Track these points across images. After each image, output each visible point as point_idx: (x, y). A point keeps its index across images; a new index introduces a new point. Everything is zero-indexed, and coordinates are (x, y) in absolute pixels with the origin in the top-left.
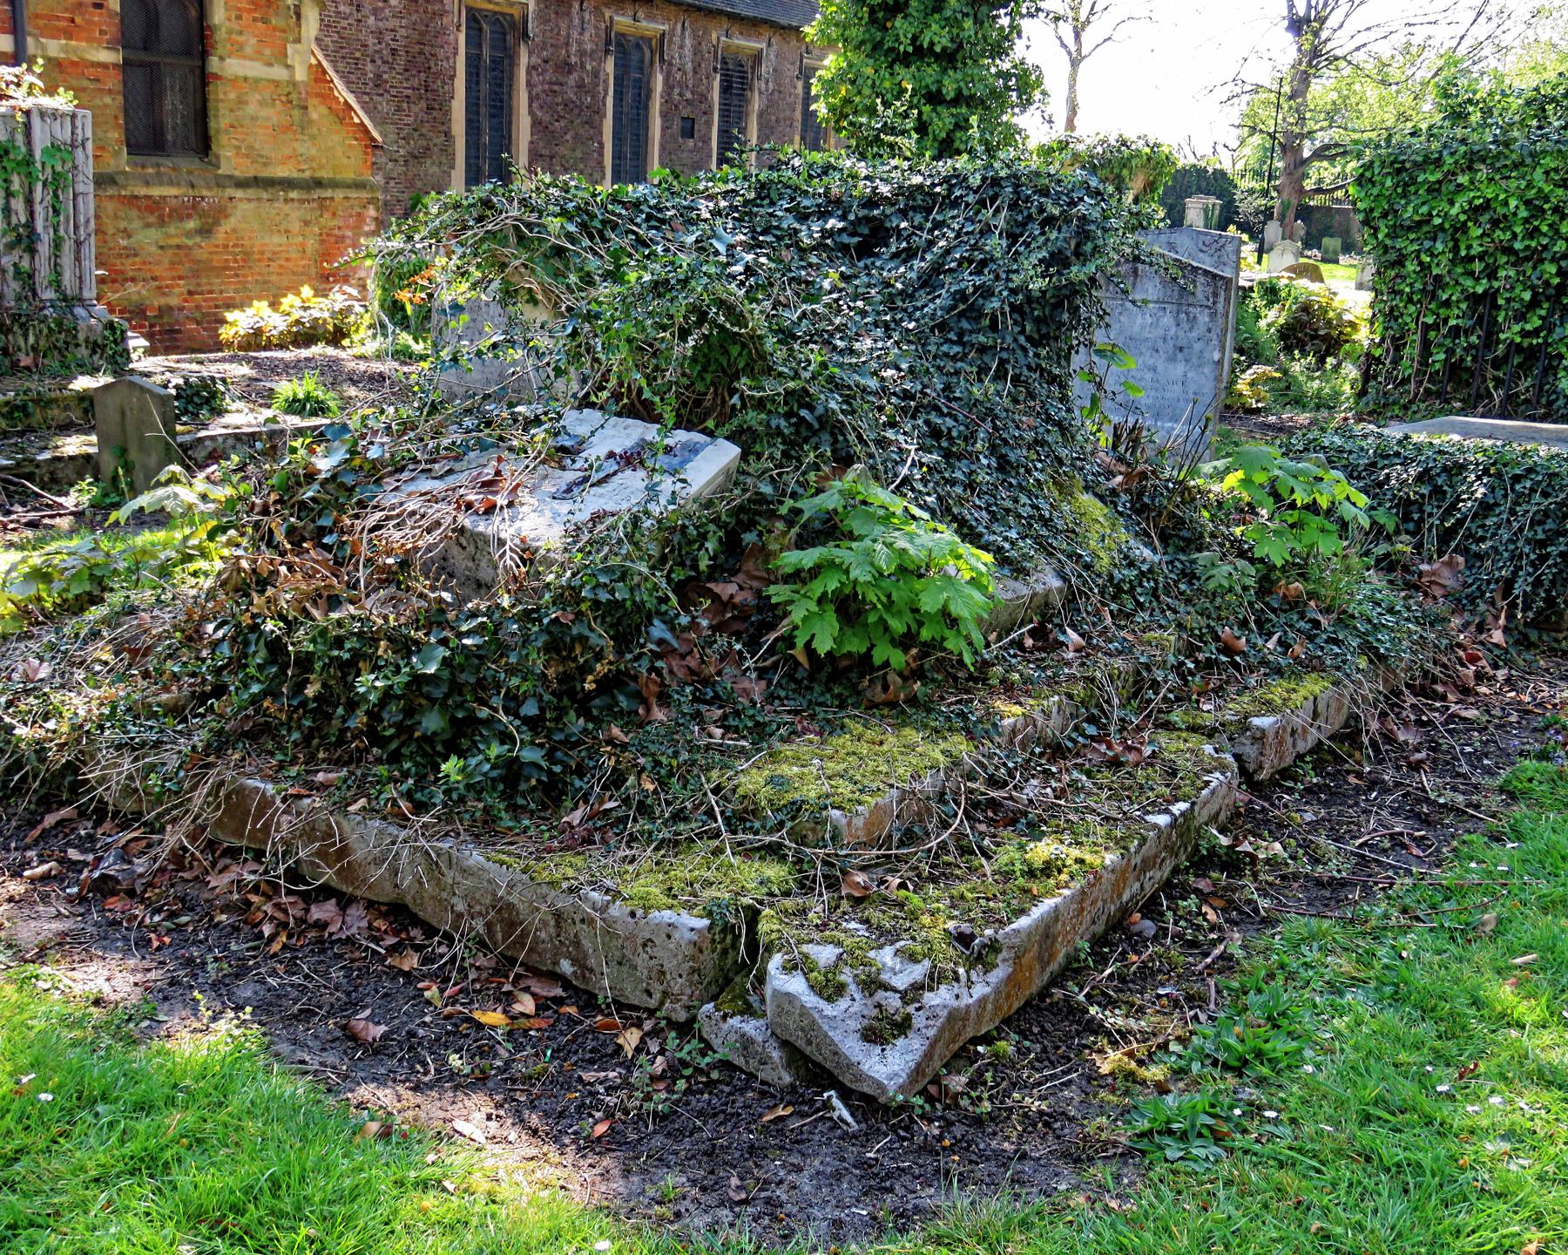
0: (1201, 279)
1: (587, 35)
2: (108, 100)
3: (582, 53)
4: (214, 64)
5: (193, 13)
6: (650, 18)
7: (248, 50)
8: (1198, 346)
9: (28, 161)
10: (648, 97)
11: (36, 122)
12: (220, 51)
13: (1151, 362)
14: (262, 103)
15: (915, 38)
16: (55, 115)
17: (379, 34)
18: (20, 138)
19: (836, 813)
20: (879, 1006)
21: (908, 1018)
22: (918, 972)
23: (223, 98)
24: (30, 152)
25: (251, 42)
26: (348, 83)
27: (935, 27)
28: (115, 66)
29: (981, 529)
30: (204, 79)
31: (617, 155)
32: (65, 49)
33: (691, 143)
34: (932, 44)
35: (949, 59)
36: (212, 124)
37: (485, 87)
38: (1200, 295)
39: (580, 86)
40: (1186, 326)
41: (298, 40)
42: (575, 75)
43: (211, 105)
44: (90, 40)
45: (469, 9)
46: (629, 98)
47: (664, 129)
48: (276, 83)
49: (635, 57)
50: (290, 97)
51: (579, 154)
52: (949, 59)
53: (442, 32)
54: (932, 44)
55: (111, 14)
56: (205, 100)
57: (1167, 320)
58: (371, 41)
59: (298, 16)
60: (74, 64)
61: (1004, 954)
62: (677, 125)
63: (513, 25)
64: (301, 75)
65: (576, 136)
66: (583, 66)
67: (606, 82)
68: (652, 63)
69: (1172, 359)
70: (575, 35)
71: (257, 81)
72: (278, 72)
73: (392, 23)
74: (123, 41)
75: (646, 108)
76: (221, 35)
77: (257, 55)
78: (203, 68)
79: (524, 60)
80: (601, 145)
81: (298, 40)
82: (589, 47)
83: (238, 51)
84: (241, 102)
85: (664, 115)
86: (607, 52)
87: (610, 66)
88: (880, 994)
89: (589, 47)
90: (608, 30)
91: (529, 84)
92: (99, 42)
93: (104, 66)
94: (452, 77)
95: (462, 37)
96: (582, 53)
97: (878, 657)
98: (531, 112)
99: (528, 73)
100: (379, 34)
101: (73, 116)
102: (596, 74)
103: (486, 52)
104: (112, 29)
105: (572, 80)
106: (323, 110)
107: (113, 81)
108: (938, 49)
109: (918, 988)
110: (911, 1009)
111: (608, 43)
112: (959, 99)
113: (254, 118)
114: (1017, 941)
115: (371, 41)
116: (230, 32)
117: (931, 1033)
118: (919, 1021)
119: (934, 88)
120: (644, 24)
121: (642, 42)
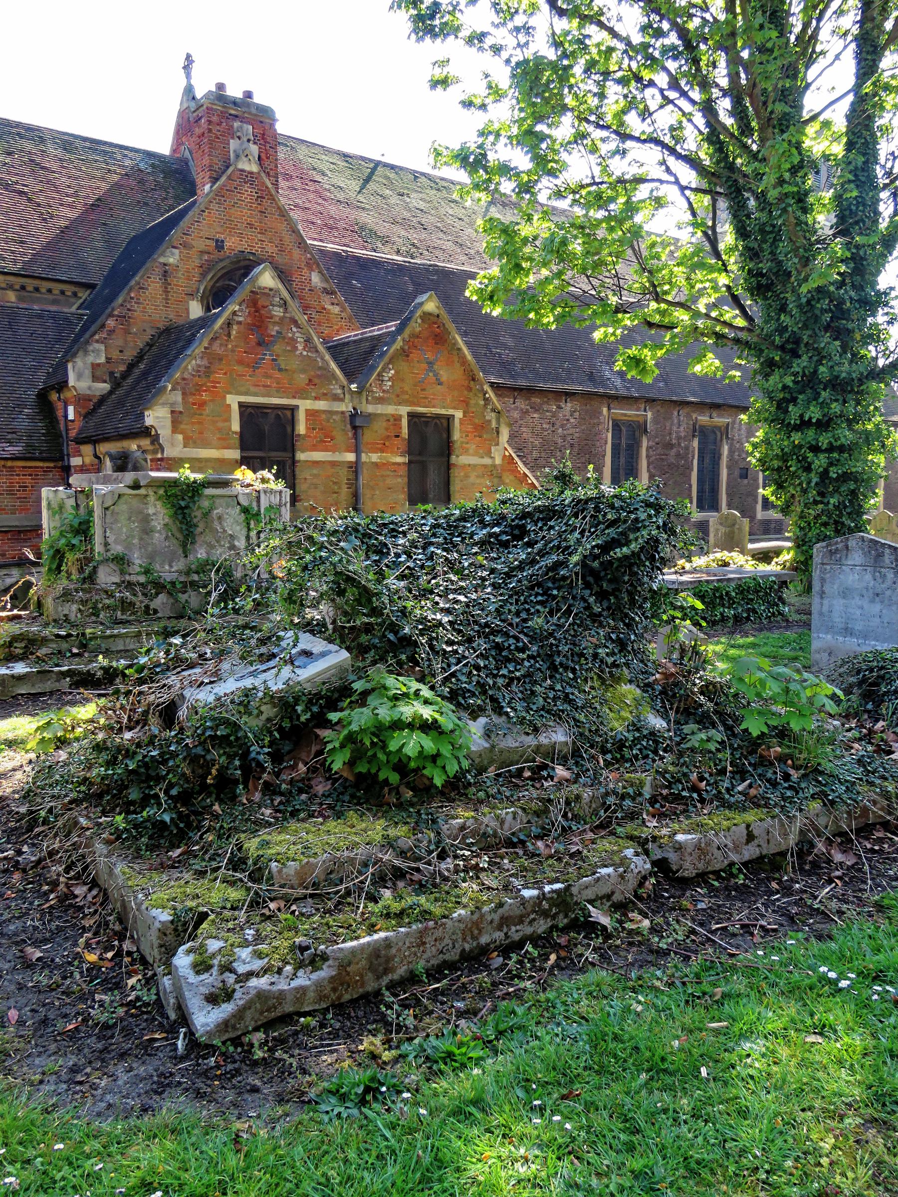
0: (887, 551)
1: (682, 429)
2: (400, 480)
3: (679, 438)
4: (453, 459)
5: (445, 436)
6: (718, 416)
7: (471, 451)
8: (888, 593)
9: (258, 514)
10: (719, 458)
11: (262, 496)
12: (457, 452)
13: (860, 603)
14: (477, 477)
15: (801, 416)
16: (272, 491)
17: (564, 437)
18: (255, 504)
19: (274, 864)
20: (223, 981)
21: (234, 991)
22: (257, 965)
23: (456, 474)
24: (259, 511)
25: (472, 447)
26: (525, 464)
27: (812, 408)
28: (404, 463)
29: (503, 704)
30: (449, 466)
31: (700, 491)
32: (380, 458)
33: (746, 481)
34: (810, 418)
35: (824, 425)
36: (452, 488)
37: (622, 460)
38: (887, 561)
39: (678, 455)
40: (880, 581)
41: (497, 444)
42: (674, 450)
43: (452, 479)
44: (392, 452)
45: (614, 421)
46: (707, 460)
47: (729, 475)
48: (485, 466)
49: (712, 437)
50: (492, 472)
51: (676, 491)
52: (824, 425)
53: (599, 433)
54: (810, 418)
55: (404, 439)
56: (449, 477)
57: (868, 577)
58: (560, 441)
59: (498, 433)
60: (384, 464)
61: (330, 962)
62: (737, 473)
63: (639, 426)
64: (498, 461)
65: (675, 482)
66: (679, 444)
67: (693, 452)
68: (721, 440)
69: (872, 601)
70: (675, 428)
71: (475, 466)
72: (487, 461)
73: (570, 432)
74: (410, 452)
75: (718, 464)
76: (457, 445)
77: (476, 454)
78: (448, 461)
79: (645, 443)
80: (691, 486)
81: (497, 444)
82: (683, 434)
83: (466, 452)
84: (467, 476)
85: (728, 467)
86: (694, 436)
87: (695, 443)
88: (227, 974)
89: (683, 434)
90: (694, 425)
91: (647, 456)
92: (397, 453)
93: (399, 464)
94: (604, 456)
95: (610, 435)
96: (679, 438)
97: (382, 776)
98: (648, 471)
99: (647, 450)
100: (564, 437)
101: (281, 492)
102: (687, 448)
103: (624, 442)
104: (403, 446)
105: (673, 452)
106: (512, 477)
107: (403, 471)
108: (814, 420)
109: (250, 974)
110: (237, 986)
111: (694, 430)
112: (831, 449)
113: (473, 484)
114: (341, 955)
115: (560, 441)
116: (462, 443)
117: (241, 1003)
118: (237, 995)
119: (814, 443)
120: (716, 419)
121: (715, 429)
